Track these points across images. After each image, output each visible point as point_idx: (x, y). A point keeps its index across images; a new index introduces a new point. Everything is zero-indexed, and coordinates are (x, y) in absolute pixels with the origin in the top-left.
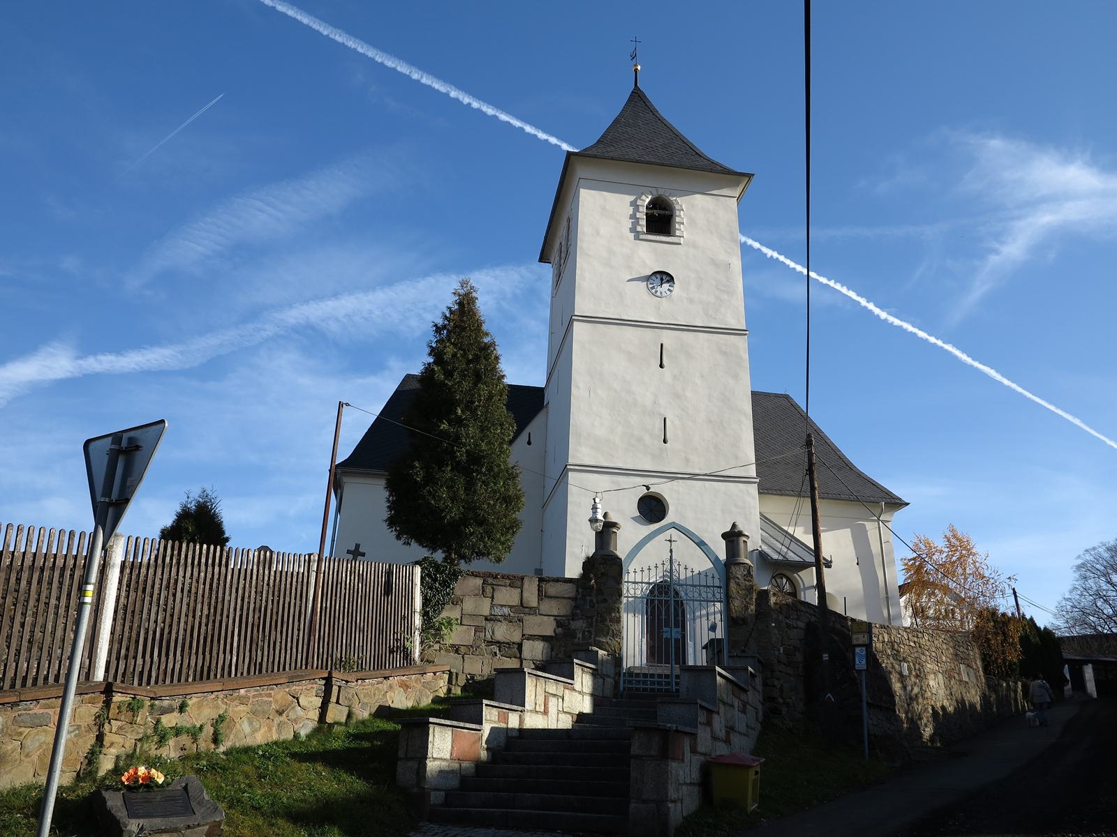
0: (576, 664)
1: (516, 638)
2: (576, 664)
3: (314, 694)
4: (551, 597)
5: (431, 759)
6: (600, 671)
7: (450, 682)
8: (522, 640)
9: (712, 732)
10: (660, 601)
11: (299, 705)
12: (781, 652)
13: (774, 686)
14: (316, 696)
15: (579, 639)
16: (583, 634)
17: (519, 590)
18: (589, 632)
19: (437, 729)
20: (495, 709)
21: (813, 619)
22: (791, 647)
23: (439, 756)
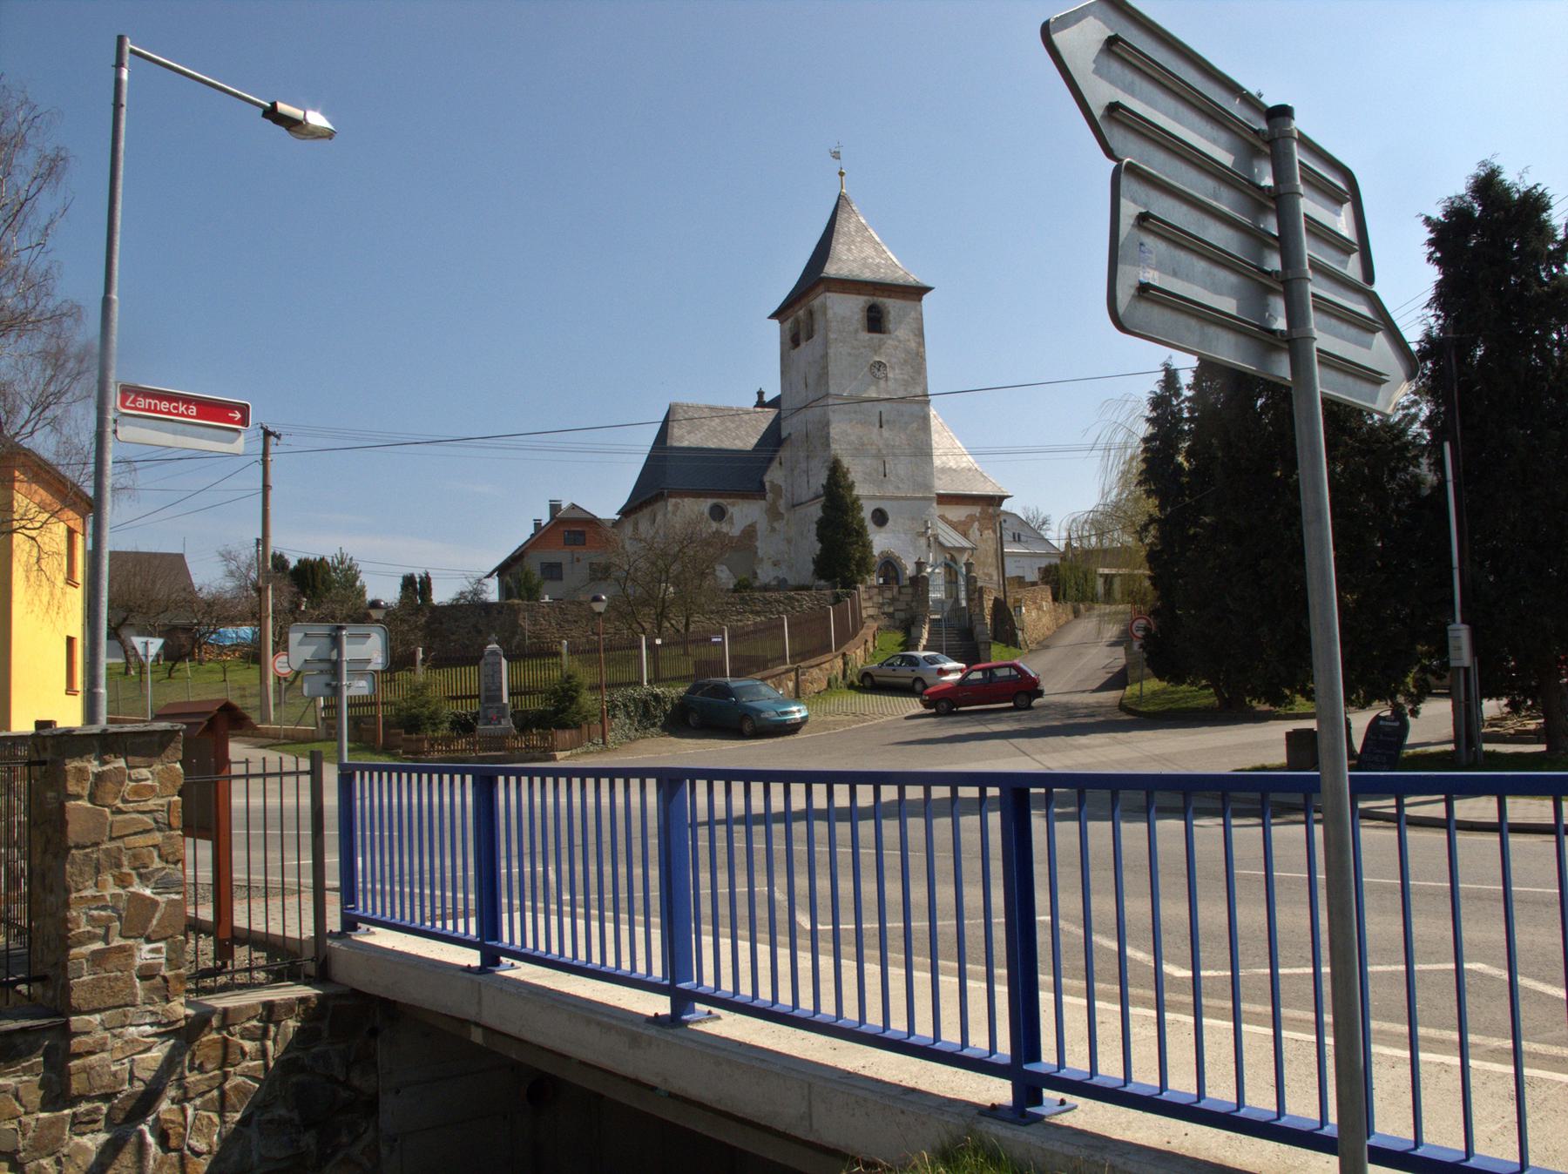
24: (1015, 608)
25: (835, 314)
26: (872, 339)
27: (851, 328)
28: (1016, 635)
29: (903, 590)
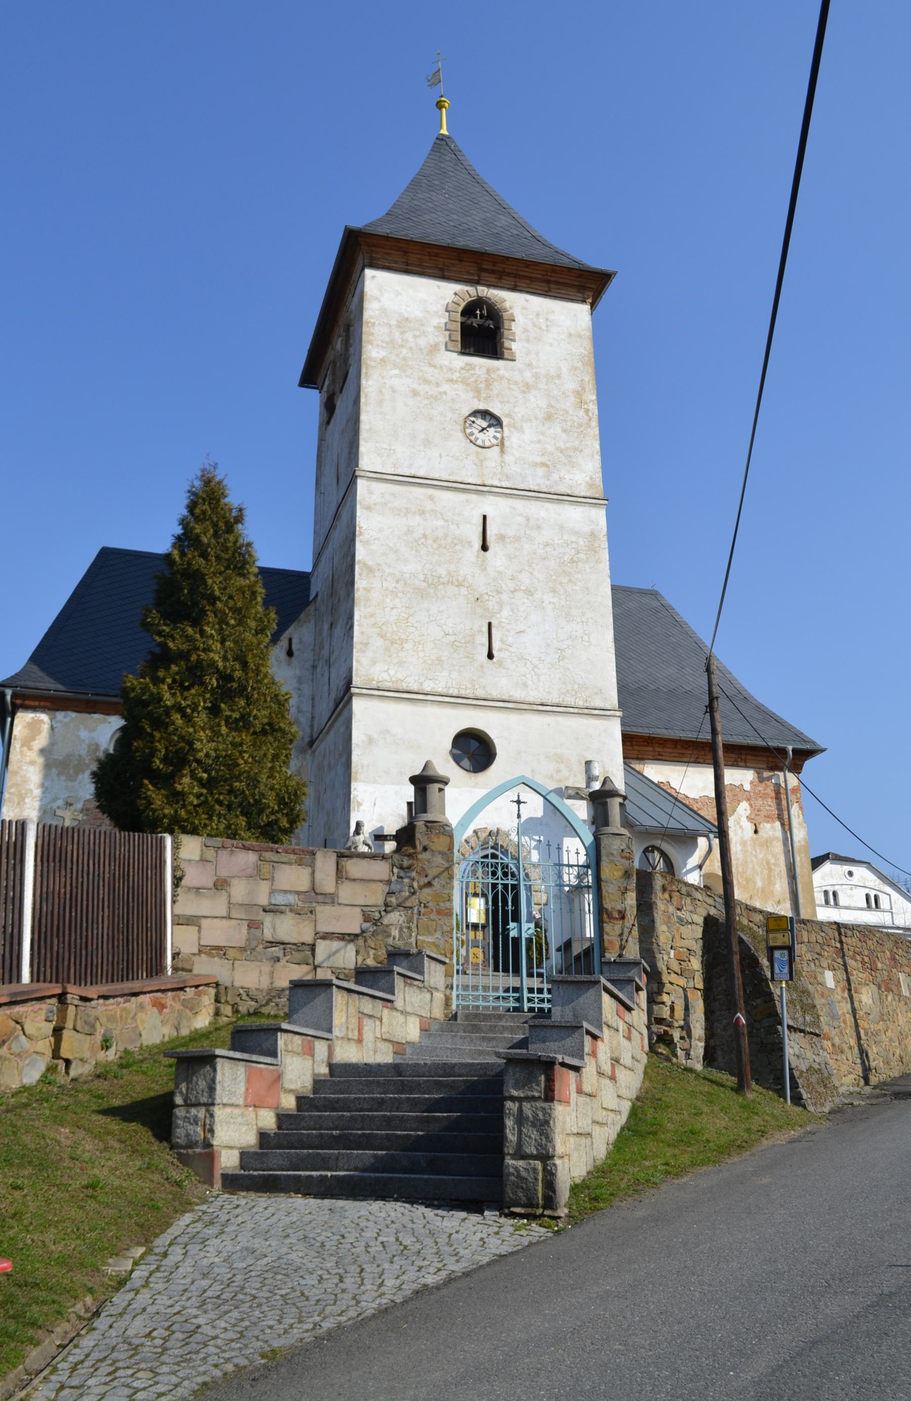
0: (398, 974)
1: (308, 938)
2: (398, 974)
3: (43, 1017)
4: (354, 880)
5: (221, 1106)
6: (426, 983)
7: (217, 1000)
8: (315, 940)
9: (597, 1066)
10: (505, 886)
11: (24, 1034)
12: (672, 956)
13: (663, 1003)
14: (46, 1020)
15: (394, 938)
16: (401, 930)
17: (309, 870)
18: (409, 928)
19: (227, 1063)
20: (297, 1037)
21: (713, 912)
22: (685, 950)
23: (230, 1102)
24: (771, 950)
25: (384, 311)
26: (471, 367)
27: (422, 342)
28: (779, 1048)
29: (353, 867)
